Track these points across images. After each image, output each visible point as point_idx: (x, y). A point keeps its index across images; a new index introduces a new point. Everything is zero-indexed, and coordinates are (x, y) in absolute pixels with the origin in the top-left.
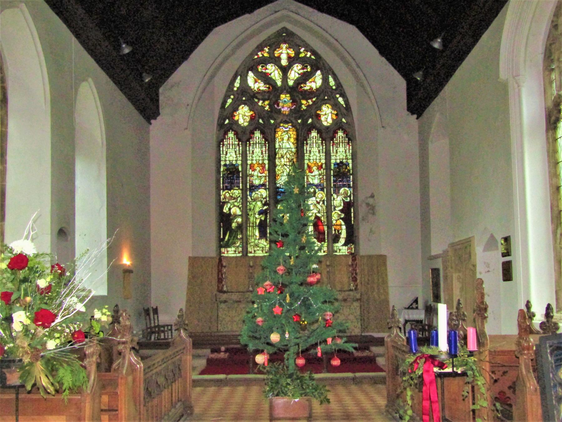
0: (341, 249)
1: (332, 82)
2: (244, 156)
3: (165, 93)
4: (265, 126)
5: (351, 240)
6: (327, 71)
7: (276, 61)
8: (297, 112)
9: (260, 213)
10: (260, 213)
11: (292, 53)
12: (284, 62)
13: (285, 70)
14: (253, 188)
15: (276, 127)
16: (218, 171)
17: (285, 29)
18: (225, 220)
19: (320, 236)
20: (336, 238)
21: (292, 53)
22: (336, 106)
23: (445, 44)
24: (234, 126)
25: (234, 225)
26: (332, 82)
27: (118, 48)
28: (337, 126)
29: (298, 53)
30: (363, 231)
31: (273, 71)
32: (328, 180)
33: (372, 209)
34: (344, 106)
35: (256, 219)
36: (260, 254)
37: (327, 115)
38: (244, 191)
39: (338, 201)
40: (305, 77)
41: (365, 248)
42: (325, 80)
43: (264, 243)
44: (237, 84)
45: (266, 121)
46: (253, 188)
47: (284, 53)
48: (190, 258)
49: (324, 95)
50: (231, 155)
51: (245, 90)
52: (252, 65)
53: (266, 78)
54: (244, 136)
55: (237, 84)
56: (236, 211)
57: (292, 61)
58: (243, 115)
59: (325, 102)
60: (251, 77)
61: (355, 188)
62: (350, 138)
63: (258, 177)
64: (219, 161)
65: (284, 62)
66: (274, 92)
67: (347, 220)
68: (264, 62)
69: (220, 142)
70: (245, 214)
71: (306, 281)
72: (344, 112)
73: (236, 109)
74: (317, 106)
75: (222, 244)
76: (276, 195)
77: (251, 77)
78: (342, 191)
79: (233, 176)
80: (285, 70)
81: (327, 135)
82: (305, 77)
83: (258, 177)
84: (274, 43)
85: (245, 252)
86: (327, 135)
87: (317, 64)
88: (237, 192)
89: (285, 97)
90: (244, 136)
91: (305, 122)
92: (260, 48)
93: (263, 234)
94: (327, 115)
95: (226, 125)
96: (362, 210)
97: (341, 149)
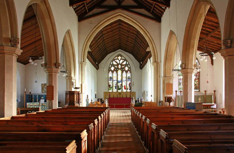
0: (129, 91)
1: (127, 63)
2: (113, 75)
3: (100, 65)
4: (116, 70)
5: (130, 89)
6: (127, 61)
7: (118, 59)
8: (121, 68)
9: (115, 85)
10: (115, 85)
11: (121, 58)
12: (120, 59)
13: (120, 61)
14: (114, 81)
15: (118, 70)
16: (108, 78)
17: (120, 54)
18: (109, 86)
19: (125, 89)
20: (128, 89)
21: (121, 58)
22: (128, 67)
23: (143, 63)
24: (111, 70)
25: (111, 87)
26: (127, 63)
27: (96, 63)
28: (128, 70)
29: (122, 58)
30: (132, 88)
31: (118, 61)
32: (127, 79)
33: (134, 84)
34: (155, 18)
35: (114, 86)
36: (115, 91)
37: (127, 68)
38: (113, 81)
39: (128, 83)
40: (123, 62)
41: (132, 91)
42: (126, 63)
43: (116, 90)
44: (112, 63)
45: (116, 69)
46: (114, 81)
47: (120, 58)
48: (104, 92)
49: (126, 65)
50: (110, 75)
51: (113, 64)
52: (114, 60)
53: (116, 62)
54: (113, 72)
55: (112, 63)
56: (111, 84)
57: (121, 59)
58: (113, 68)
59: (126, 66)
60: (114, 62)
61: (131, 81)
62: (131, 72)
63: (115, 79)
64: (108, 76)
65: (120, 59)
66: (118, 65)
67: (130, 86)
68: (116, 59)
69: (109, 72)
70: (113, 85)
71: (19, 102)
72: (130, 68)
73: (111, 67)
74: (125, 67)
75: (109, 90)
76: (118, 82)
77: (114, 62)
78: (129, 81)
79: (111, 78)
80: (120, 61)
81: (127, 72)
82: (123, 62)
83: (115, 79)
84: (118, 56)
85: (113, 91)
86: (127, 72)
87: (125, 60)
88: (111, 81)
89: (120, 66)
90: (113, 72)
91: (123, 70)
92: (116, 57)
93: (116, 88)
94: (127, 68)
95: (109, 70)
96: (132, 84)
97: (129, 74)
